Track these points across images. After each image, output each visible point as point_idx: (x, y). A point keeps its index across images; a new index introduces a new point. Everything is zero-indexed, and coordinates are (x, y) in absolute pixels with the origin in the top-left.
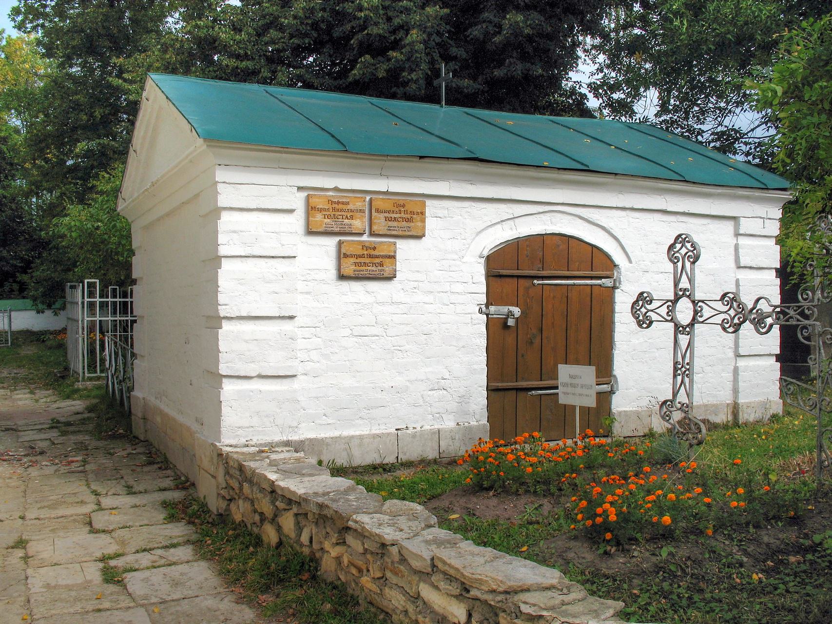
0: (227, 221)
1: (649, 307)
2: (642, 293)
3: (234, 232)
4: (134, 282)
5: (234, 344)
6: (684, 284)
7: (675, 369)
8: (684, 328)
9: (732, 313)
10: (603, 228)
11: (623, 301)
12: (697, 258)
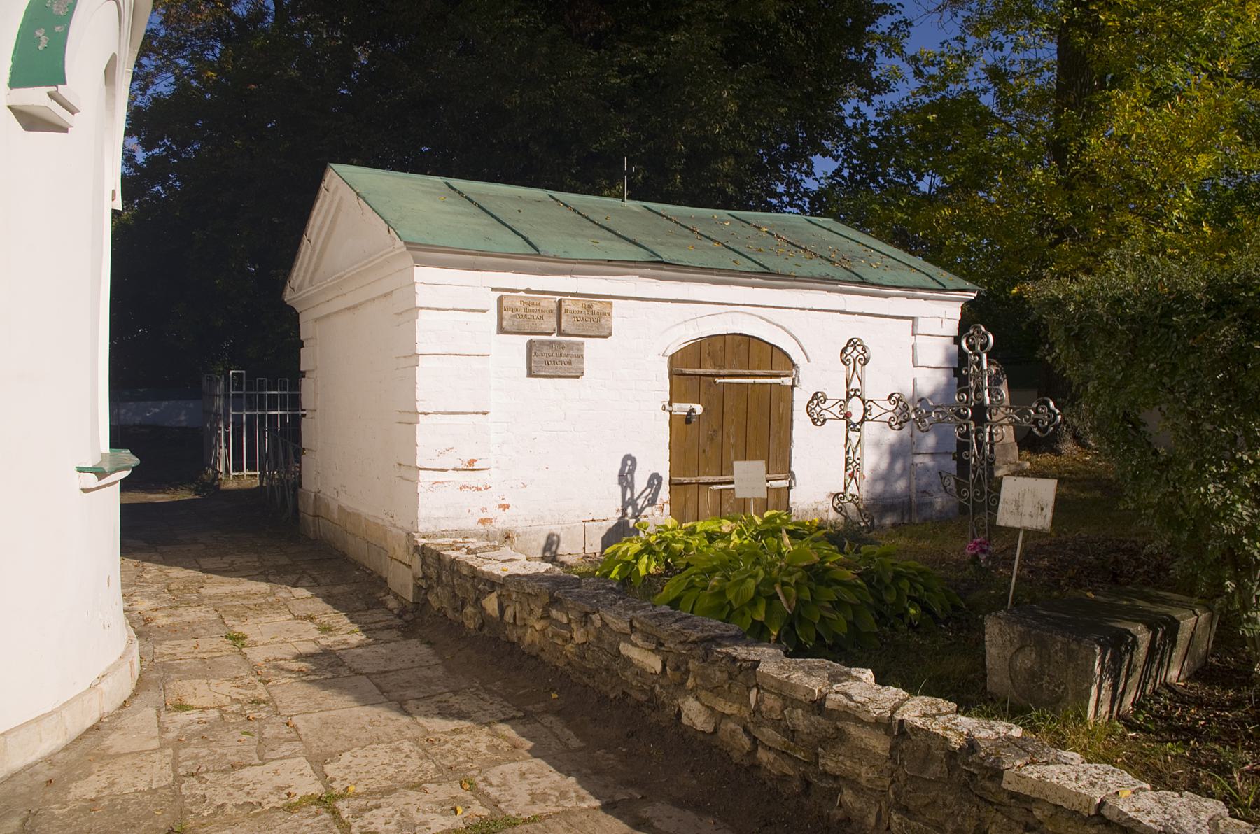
0: (423, 319)
1: (823, 406)
2: (816, 394)
3: (430, 331)
4: (303, 374)
5: (431, 440)
6: (855, 384)
7: (847, 464)
8: (855, 425)
9: (818, 409)
10: (784, 328)
11: (801, 398)
12: (866, 361)
